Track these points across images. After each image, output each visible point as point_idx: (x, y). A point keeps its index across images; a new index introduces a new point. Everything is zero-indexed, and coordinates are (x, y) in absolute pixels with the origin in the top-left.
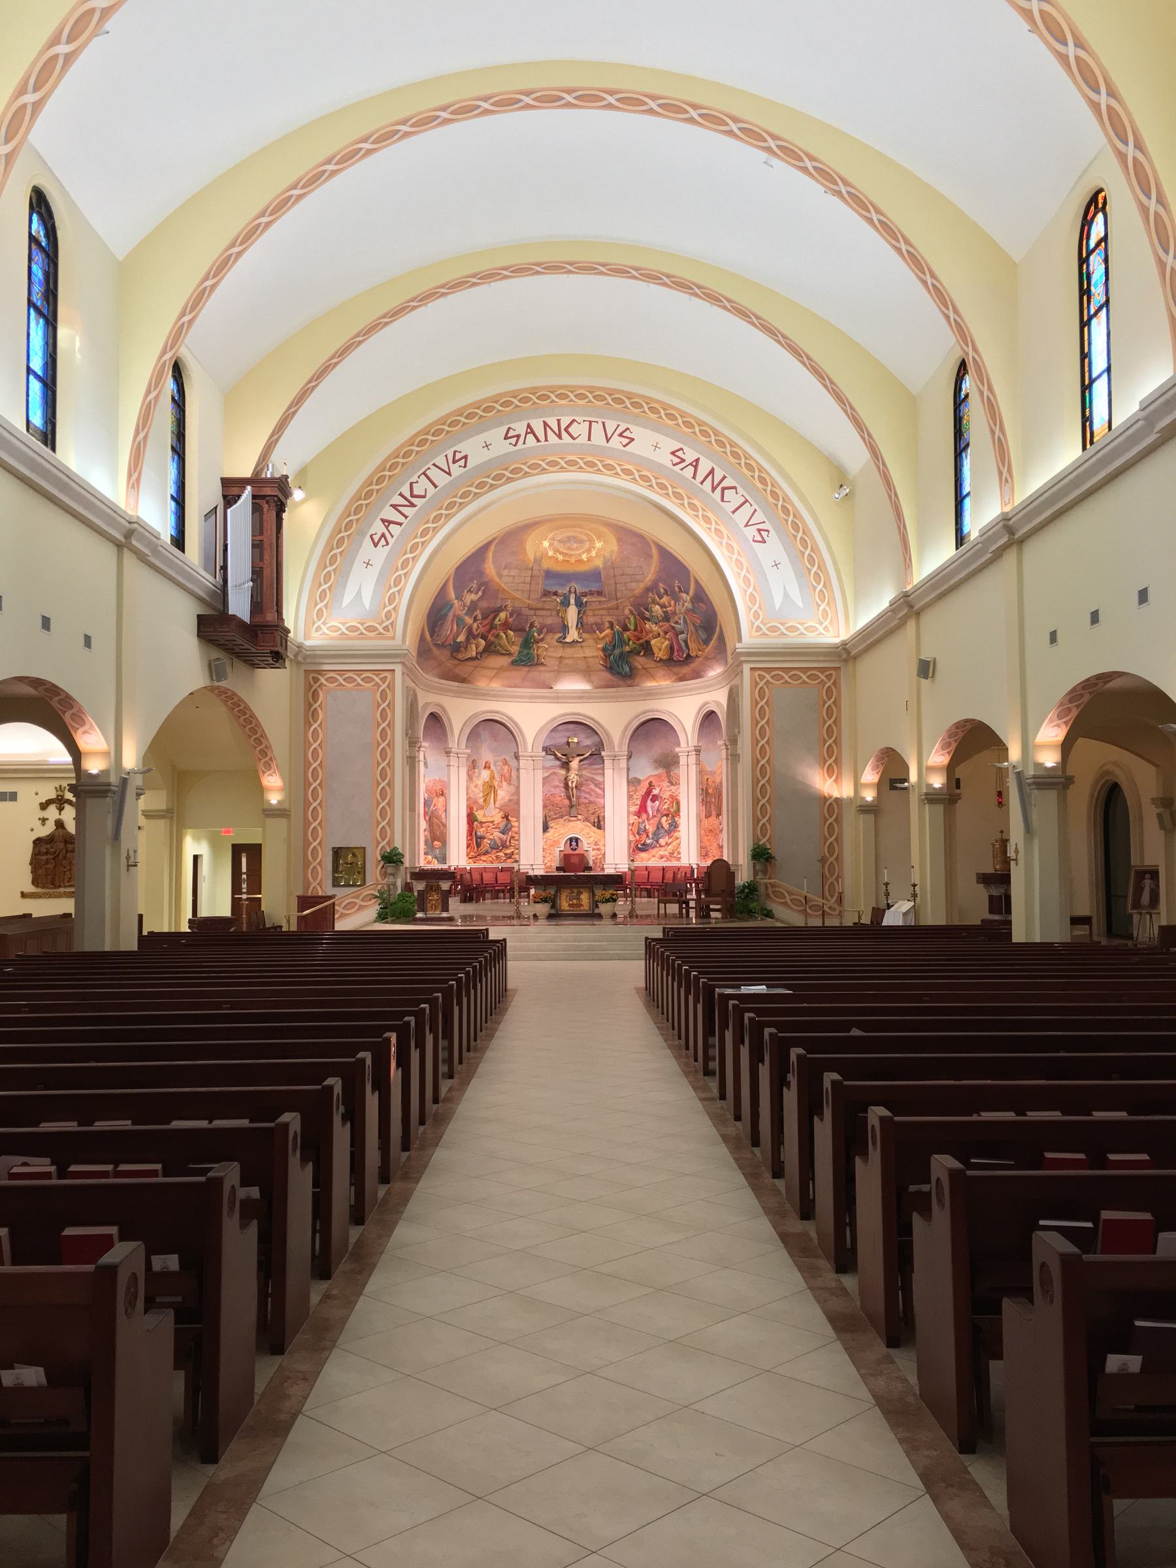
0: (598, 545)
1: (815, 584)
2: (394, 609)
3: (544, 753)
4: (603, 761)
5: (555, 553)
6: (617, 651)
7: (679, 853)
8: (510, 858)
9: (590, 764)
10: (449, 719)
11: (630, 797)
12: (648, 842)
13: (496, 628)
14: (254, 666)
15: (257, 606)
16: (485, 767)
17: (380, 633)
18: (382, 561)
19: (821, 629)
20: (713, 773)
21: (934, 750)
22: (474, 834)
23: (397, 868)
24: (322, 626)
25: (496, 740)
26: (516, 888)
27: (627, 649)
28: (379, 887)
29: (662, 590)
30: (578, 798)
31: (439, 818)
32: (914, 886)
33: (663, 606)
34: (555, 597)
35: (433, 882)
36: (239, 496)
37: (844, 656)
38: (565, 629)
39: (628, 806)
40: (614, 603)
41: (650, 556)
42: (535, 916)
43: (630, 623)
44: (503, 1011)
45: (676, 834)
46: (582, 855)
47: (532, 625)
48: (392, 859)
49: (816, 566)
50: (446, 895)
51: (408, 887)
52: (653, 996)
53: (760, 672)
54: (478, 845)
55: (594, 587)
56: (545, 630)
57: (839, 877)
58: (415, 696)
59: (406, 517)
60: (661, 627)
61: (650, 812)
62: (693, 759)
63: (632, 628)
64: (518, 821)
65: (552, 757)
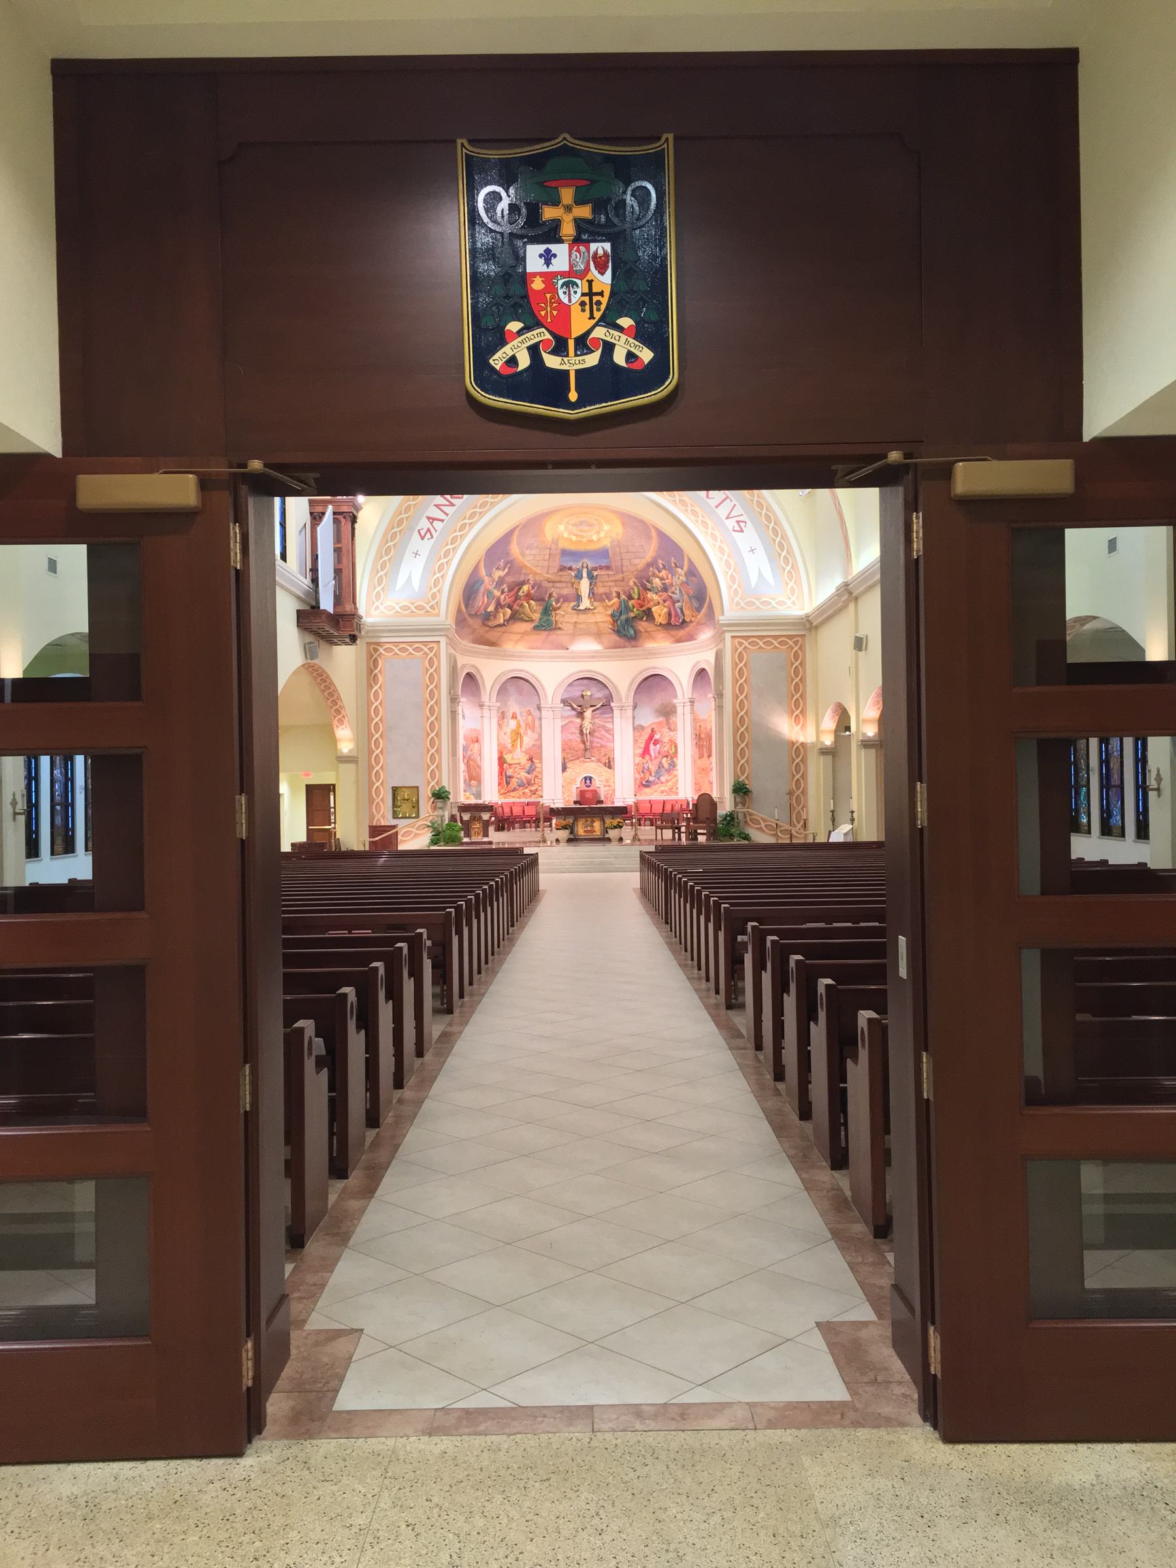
0: (606, 528)
1: (784, 566)
2: (439, 591)
3: (562, 705)
4: (613, 711)
5: (569, 534)
6: (623, 617)
7: (677, 788)
8: (535, 794)
9: (602, 714)
10: (482, 677)
11: (635, 741)
12: (651, 779)
13: (520, 599)
14: (333, 643)
15: (338, 600)
16: (512, 717)
17: (428, 611)
18: (428, 551)
19: (789, 603)
20: (705, 721)
21: (867, 707)
22: (504, 773)
23: (445, 803)
24: (380, 606)
25: (521, 695)
26: (542, 817)
27: (632, 615)
28: (431, 818)
29: (661, 565)
30: (592, 743)
31: (475, 761)
32: (852, 812)
33: (662, 579)
34: (570, 572)
35: (477, 814)
36: (323, 514)
37: (808, 626)
38: (578, 598)
39: (634, 749)
40: (620, 576)
41: (650, 537)
42: (557, 840)
43: (634, 593)
44: (538, 901)
45: (674, 773)
46: (595, 791)
47: (550, 596)
48: (440, 796)
49: (785, 551)
50: (486, 824)
51: (453, 818)
52: (645, 892)
53: (741, 640)
54: (508, 783)
55: (604, 563)
56: (561, 600)
57: (804, 807)
58: (455, 658)
59: (447, 515)
60: (661, 596)
61: (653, 754)
62: (688, 708)
63: (636, 597)
64: (541, 763)
65: (569, 708)
